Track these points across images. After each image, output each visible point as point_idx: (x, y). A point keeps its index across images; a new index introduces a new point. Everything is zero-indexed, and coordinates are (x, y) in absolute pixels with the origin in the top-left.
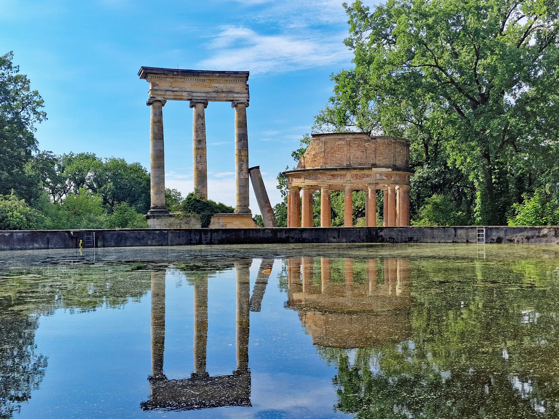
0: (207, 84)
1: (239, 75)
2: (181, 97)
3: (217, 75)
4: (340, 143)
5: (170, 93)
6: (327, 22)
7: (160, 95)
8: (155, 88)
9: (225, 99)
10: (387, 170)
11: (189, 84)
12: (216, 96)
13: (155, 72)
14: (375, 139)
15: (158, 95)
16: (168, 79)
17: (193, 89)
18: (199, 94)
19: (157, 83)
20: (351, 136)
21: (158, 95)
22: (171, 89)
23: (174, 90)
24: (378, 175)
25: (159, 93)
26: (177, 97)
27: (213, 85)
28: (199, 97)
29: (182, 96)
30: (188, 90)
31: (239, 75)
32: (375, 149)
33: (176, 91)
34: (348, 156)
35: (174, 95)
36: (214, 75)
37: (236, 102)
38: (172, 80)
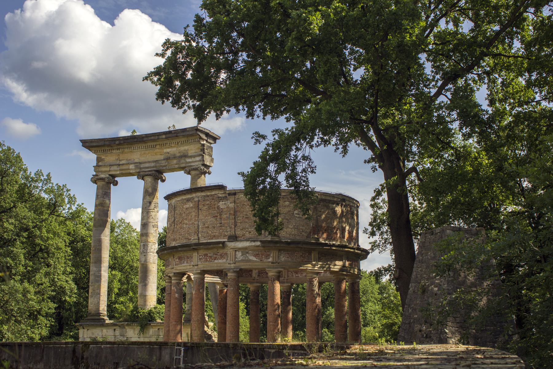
0: (158, 151)
1: (187, 133)
2: (128, 171)
3: (164, 136)
4: (188, 206)
5: (115, 168)
6: (26, 91)
7: (105, 172)
8: (100, 164)
9: (177, 166)
10: (253, 244)
11: (138, 155)
12: (167, 164)
13: (94, 144)
14: (235, 194)
15: (102, 172)
16: (114, 151)
17: (143, 159)
18: (147, 165)
19: (103, 157)
20: (199, 194)
21: (102, 172)
22: (118, 162)
23: (121, 163)
24: (239, 254)
25: (103, 169)
26: (124, 172)
27: (165, 151)
28: (148, 168)
29: (129, 169)
30: (136, 161)
31: (187, 133)
32: (235, 212)
33: (123, 164)
34: (196, 226)
35: (120, 170)
36: (161, 137)
37: (187, 169)
38: (118, 151)
